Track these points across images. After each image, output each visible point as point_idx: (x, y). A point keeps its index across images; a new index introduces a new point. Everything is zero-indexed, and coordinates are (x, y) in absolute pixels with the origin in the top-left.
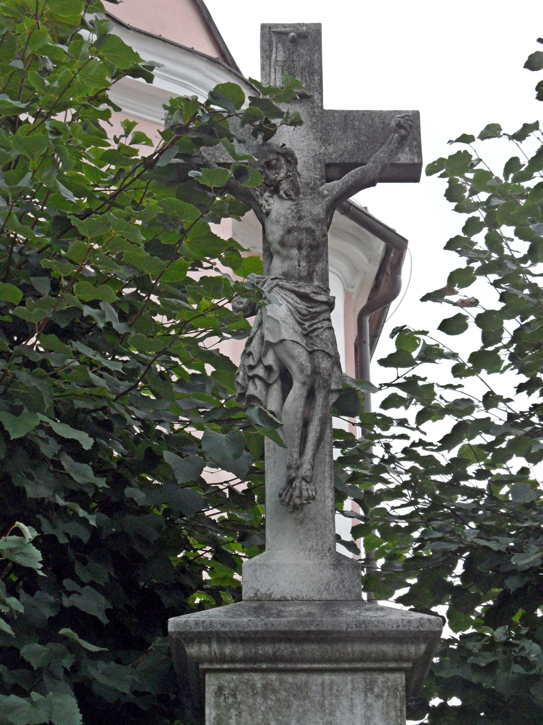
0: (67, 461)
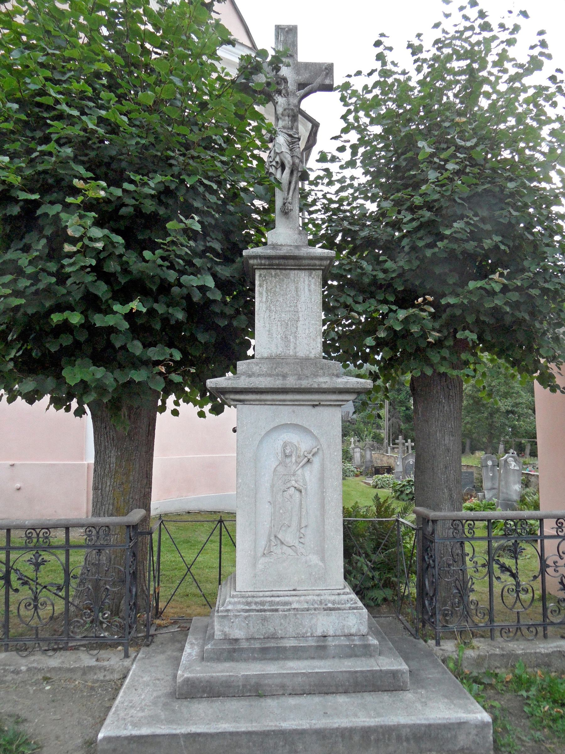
0: (207, 195)
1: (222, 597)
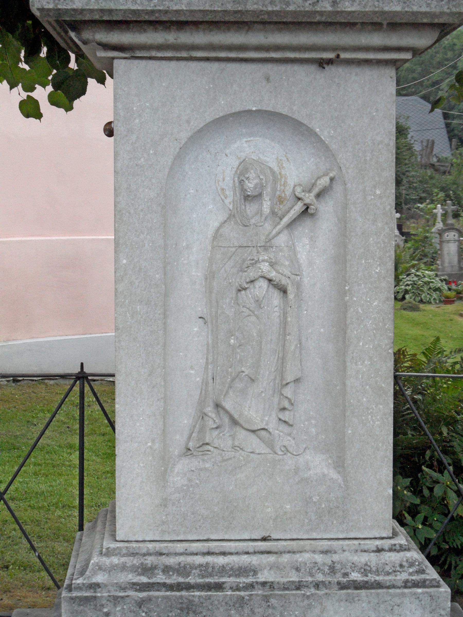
1: (82, 557)
